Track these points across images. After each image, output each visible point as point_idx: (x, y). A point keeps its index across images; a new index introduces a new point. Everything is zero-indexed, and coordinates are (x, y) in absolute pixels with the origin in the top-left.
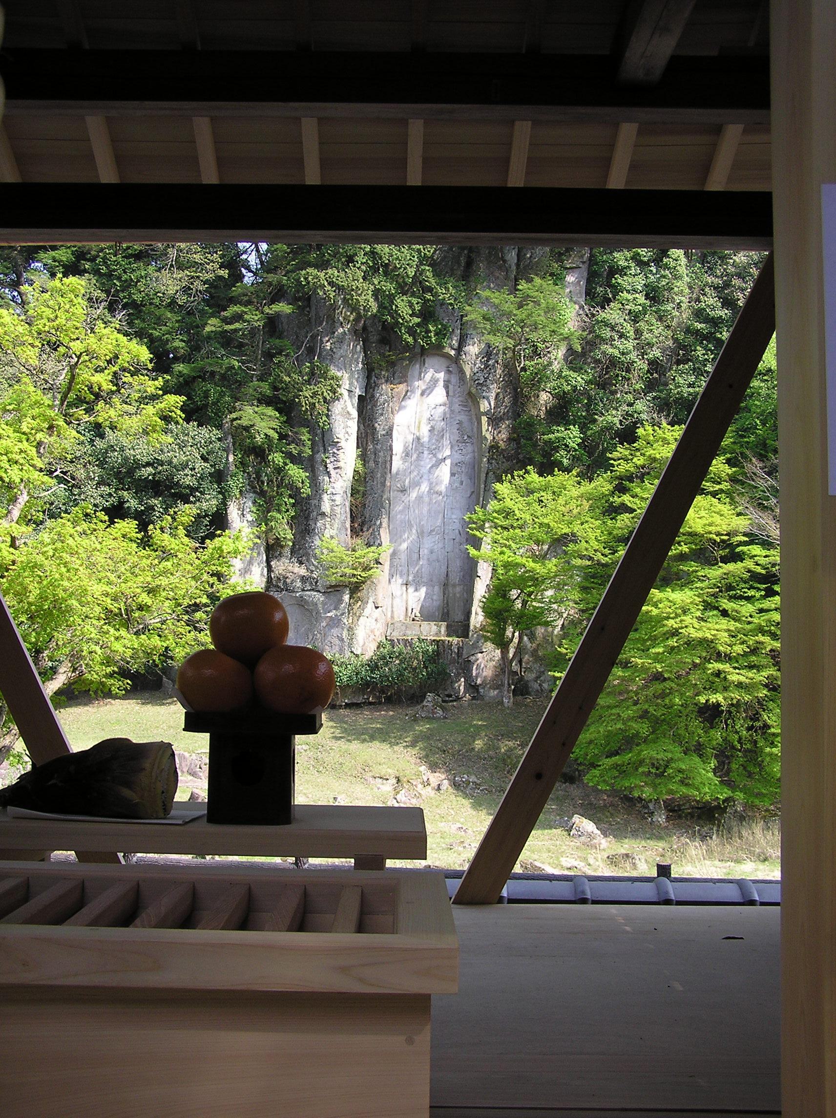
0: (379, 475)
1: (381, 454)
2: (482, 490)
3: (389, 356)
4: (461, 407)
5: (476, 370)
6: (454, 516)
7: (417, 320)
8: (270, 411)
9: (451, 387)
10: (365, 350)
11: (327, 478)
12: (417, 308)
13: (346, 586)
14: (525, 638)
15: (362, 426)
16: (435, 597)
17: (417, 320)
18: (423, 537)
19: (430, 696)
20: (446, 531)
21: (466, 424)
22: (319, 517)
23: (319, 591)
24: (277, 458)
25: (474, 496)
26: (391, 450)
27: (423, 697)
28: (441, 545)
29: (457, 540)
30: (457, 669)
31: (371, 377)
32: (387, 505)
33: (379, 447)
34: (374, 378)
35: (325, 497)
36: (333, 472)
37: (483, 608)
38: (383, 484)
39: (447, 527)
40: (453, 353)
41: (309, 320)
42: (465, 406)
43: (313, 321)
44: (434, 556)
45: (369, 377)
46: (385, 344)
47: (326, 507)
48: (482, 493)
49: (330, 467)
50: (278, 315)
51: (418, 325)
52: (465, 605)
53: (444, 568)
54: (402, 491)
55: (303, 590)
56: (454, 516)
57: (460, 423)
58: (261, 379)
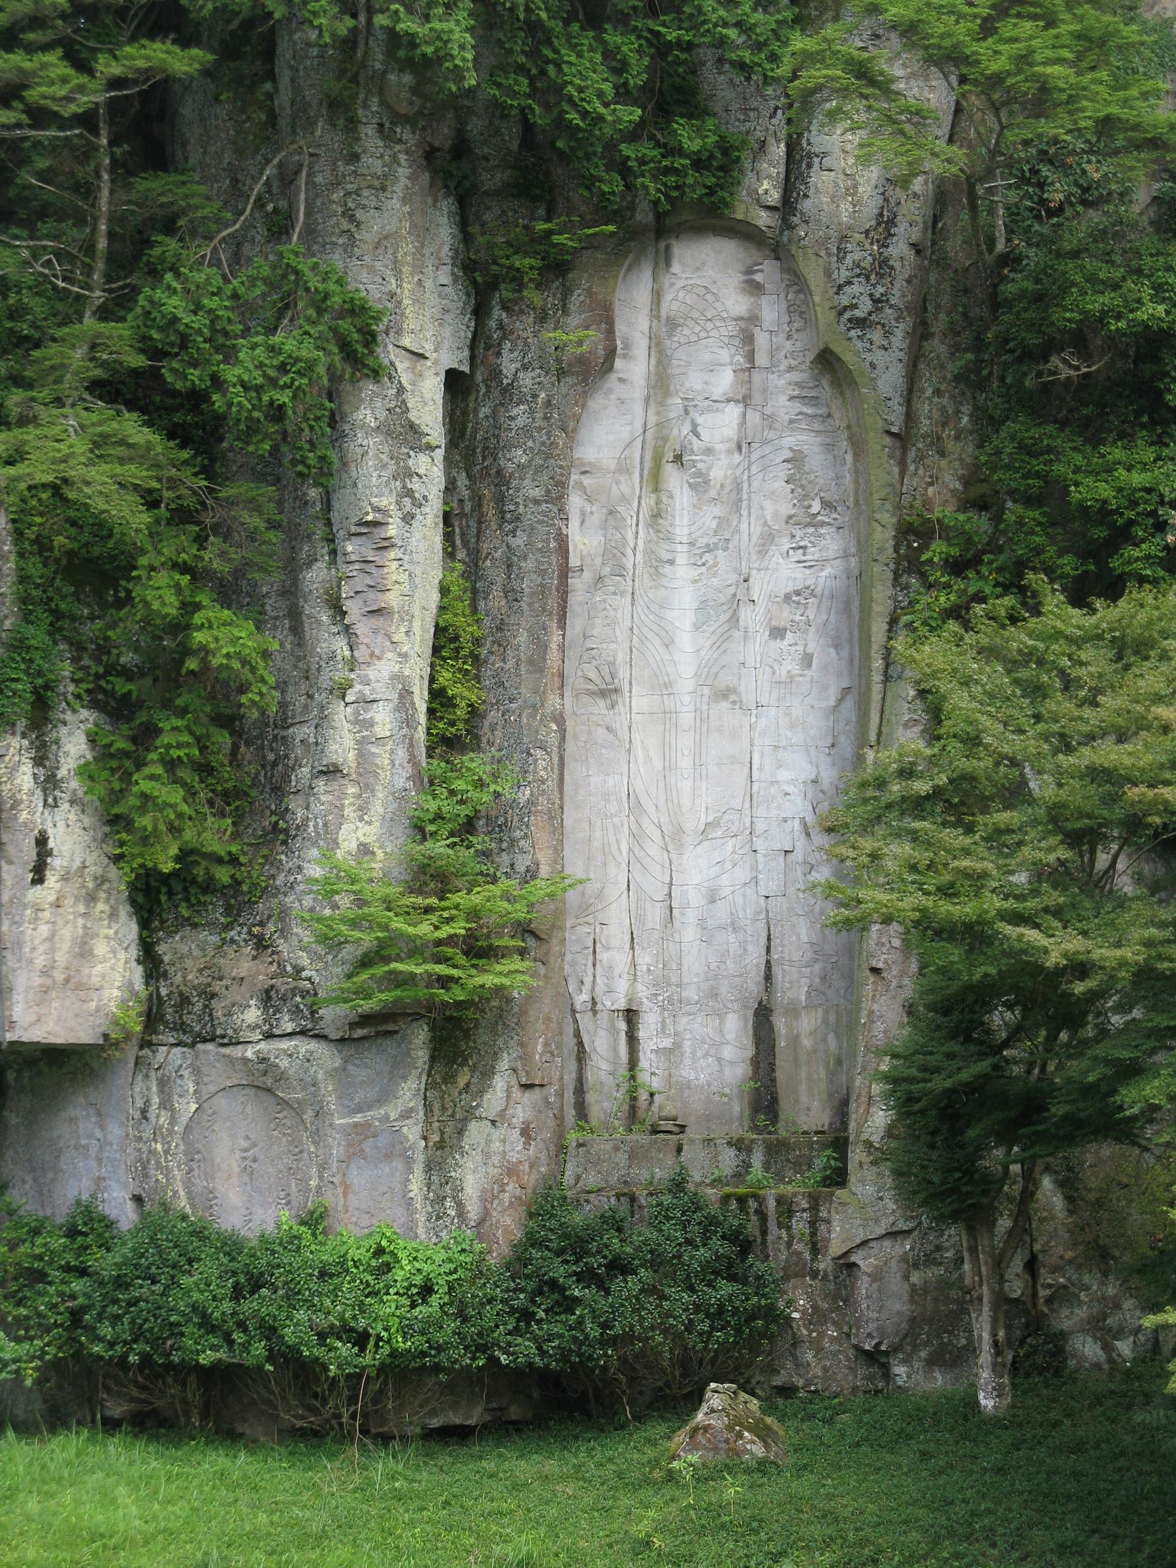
0: (523, 637)
1: (529, 564)
2: (877, 678)
3: (549, 233)
4: (797, 406)
5: (844, 275)
6: (783, 775)
7: (632, 114)
8: (133, 428)
9: (762, 339)
10: (463, 223)
11: (340, 646)
12: (636, 78)
13: (416, 1017)
14: (1047, 1182)
15: (462, 481)
16: (728, 1053)
17: (632, 114)
18: (680, 846)
19: (716, 1397)
20: (760, 827)
21: (816, 460)
22: (321, 784)
23: (324, 1037)
24: (160, 593)
25: (849, 704)
26: (563, 549)
27: (695, 1398)
28: (742, 874)
29: (798, 856)
30: (810, 1297)
31: (484, 288)
32: (553, 740)
33: (519, 541)
34: (497, 313)
35: (341, 714)
36: (362, 629)
37: (894, 1080)
38: (537, 664)
39: (760, 812)
40: (763, 219)
41: (273, 116)
42: (813, 401)
43: (283, 123)
44: (721, 912)
45: (480, 312)
46: (535, 199)
47: (342, 746)
48: (877, 688)
49: (353, 609)
50: (726, 36)
51: (634, 134)
52: (832, 1075)
53: (755, 956)
54: (603, 694)
55: (269, 1036)
56: (783, 775)
57: (796, 459)
58: (105, 314)
